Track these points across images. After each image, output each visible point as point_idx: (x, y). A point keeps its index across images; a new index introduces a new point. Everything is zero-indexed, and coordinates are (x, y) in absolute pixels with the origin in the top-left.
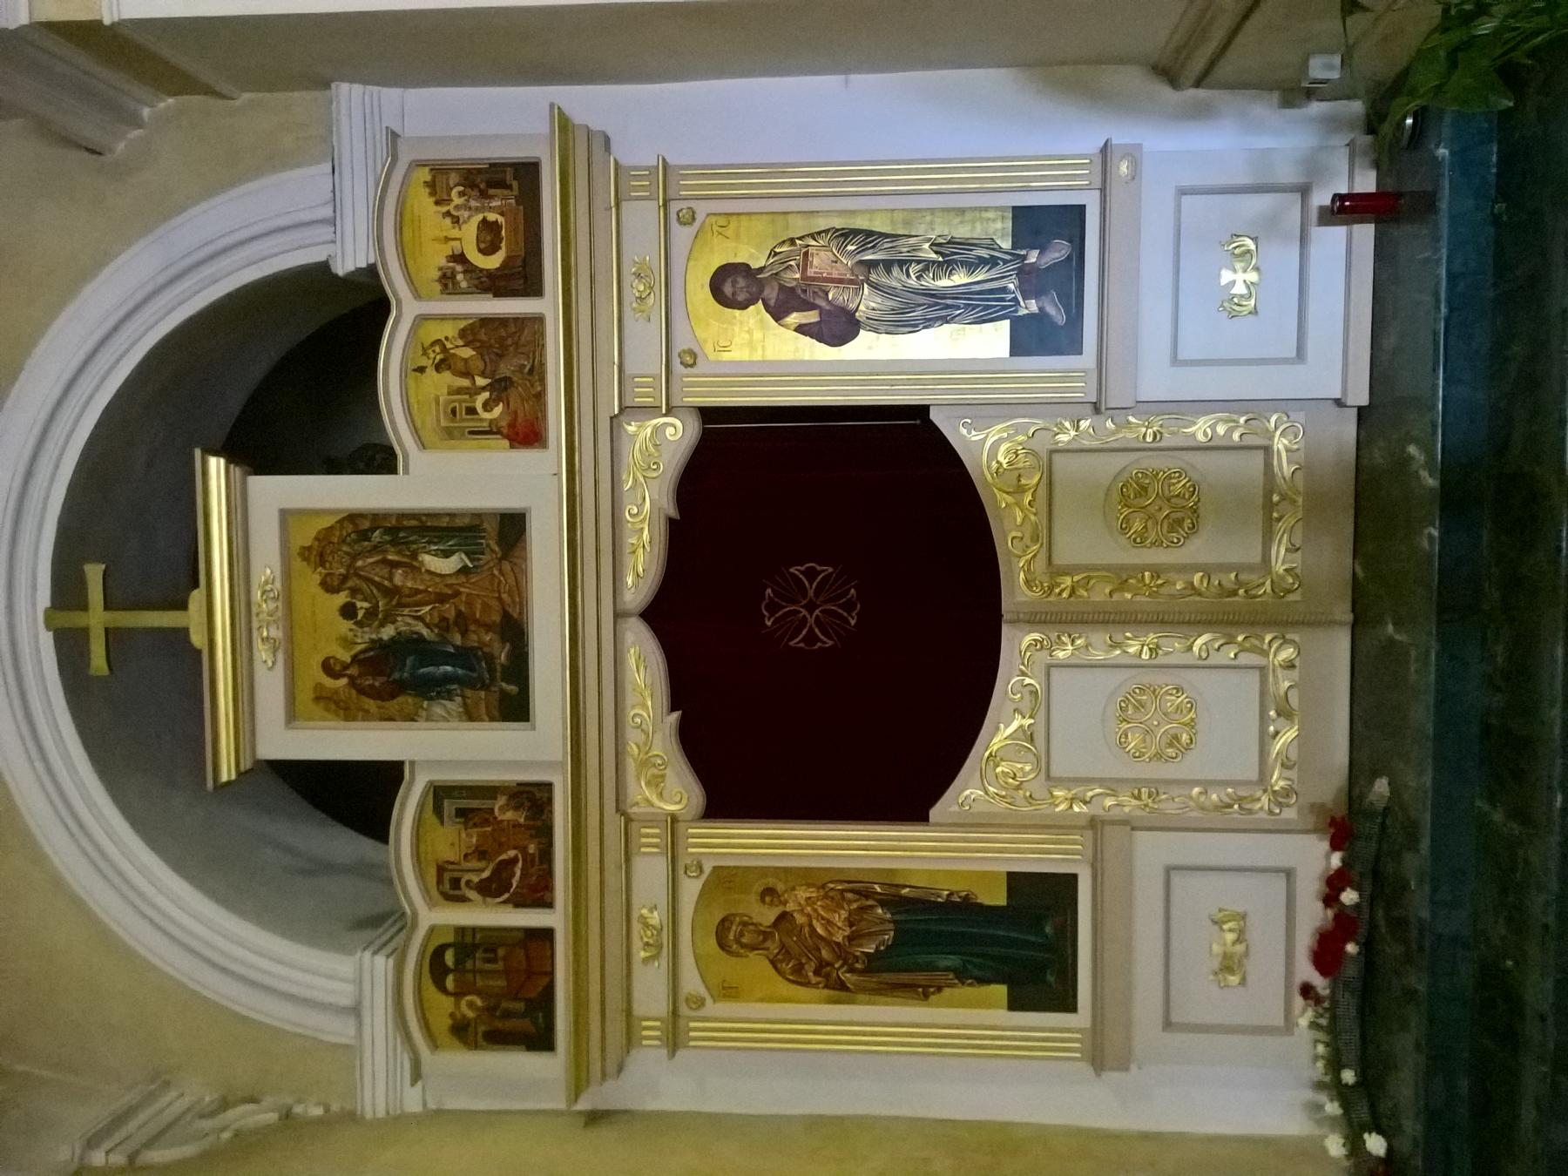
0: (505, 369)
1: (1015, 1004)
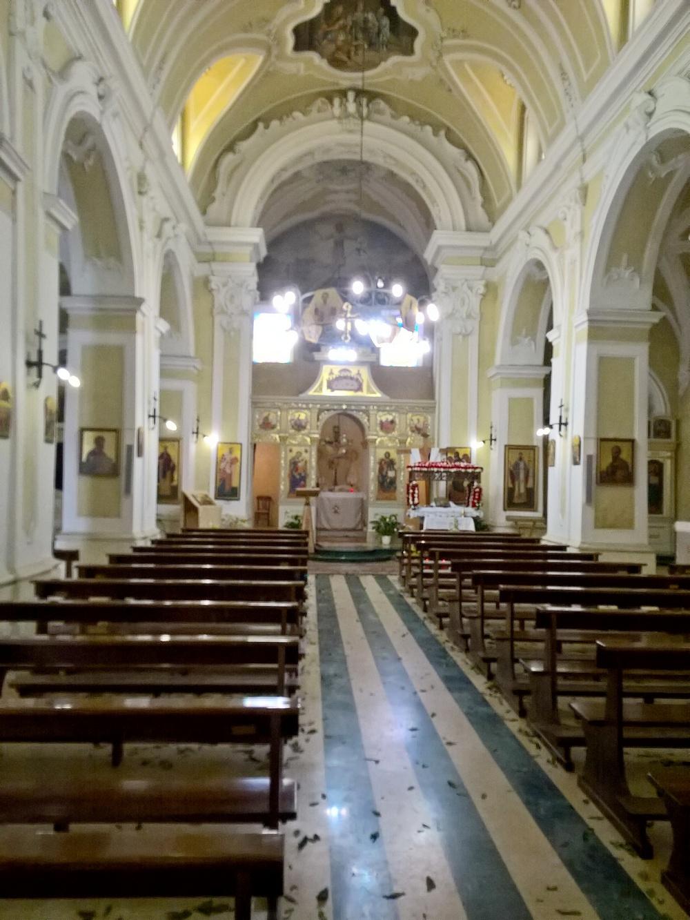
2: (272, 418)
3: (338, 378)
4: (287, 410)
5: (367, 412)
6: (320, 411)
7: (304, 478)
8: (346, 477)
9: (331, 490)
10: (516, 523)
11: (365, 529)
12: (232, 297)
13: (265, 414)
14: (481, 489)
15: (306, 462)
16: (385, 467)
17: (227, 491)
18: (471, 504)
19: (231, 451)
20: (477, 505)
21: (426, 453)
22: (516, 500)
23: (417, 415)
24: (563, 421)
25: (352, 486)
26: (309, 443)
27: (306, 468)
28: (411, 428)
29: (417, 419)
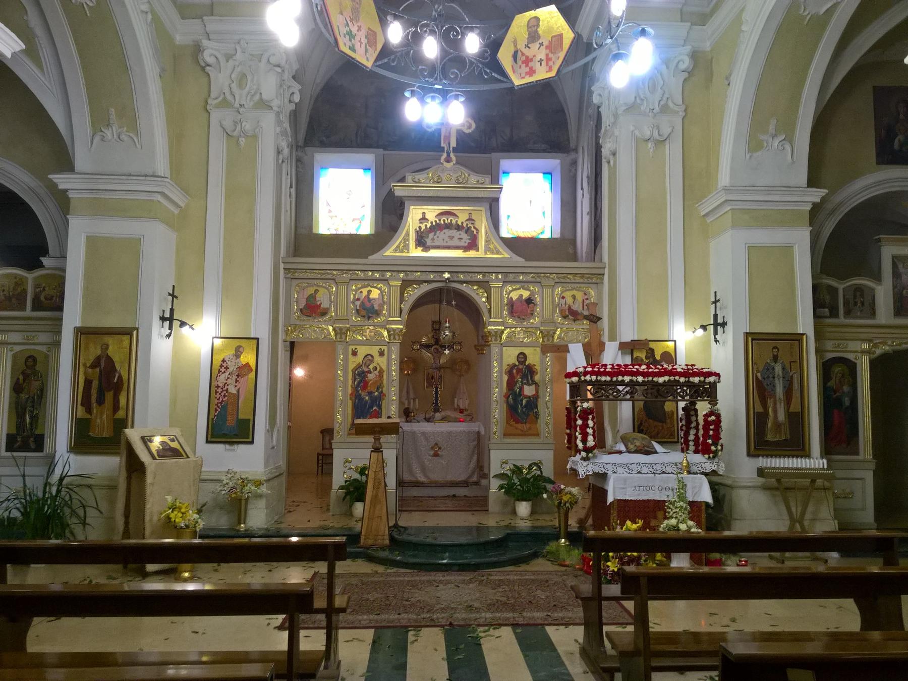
0: (14, 301)
1: (8, 435)
2: (323, 298)
3: (436, 228)
4: (347, 283)
5: (484, 285)
8: (454, 397)
9: (428, 420)
10: (779, 481)
11: (484, 482)
13: (311, 291)
14: (718, 416)
17: (228, 427)
18: (692, 448)
19: (238, 353)
20: (713, 448)
21: (592, 351)
22: (770, 437)
23: (573, 289)
24: (720, 320)
25: (461, 411)
27: (381, 383)
28: (561, 311)
29: (574, 297)
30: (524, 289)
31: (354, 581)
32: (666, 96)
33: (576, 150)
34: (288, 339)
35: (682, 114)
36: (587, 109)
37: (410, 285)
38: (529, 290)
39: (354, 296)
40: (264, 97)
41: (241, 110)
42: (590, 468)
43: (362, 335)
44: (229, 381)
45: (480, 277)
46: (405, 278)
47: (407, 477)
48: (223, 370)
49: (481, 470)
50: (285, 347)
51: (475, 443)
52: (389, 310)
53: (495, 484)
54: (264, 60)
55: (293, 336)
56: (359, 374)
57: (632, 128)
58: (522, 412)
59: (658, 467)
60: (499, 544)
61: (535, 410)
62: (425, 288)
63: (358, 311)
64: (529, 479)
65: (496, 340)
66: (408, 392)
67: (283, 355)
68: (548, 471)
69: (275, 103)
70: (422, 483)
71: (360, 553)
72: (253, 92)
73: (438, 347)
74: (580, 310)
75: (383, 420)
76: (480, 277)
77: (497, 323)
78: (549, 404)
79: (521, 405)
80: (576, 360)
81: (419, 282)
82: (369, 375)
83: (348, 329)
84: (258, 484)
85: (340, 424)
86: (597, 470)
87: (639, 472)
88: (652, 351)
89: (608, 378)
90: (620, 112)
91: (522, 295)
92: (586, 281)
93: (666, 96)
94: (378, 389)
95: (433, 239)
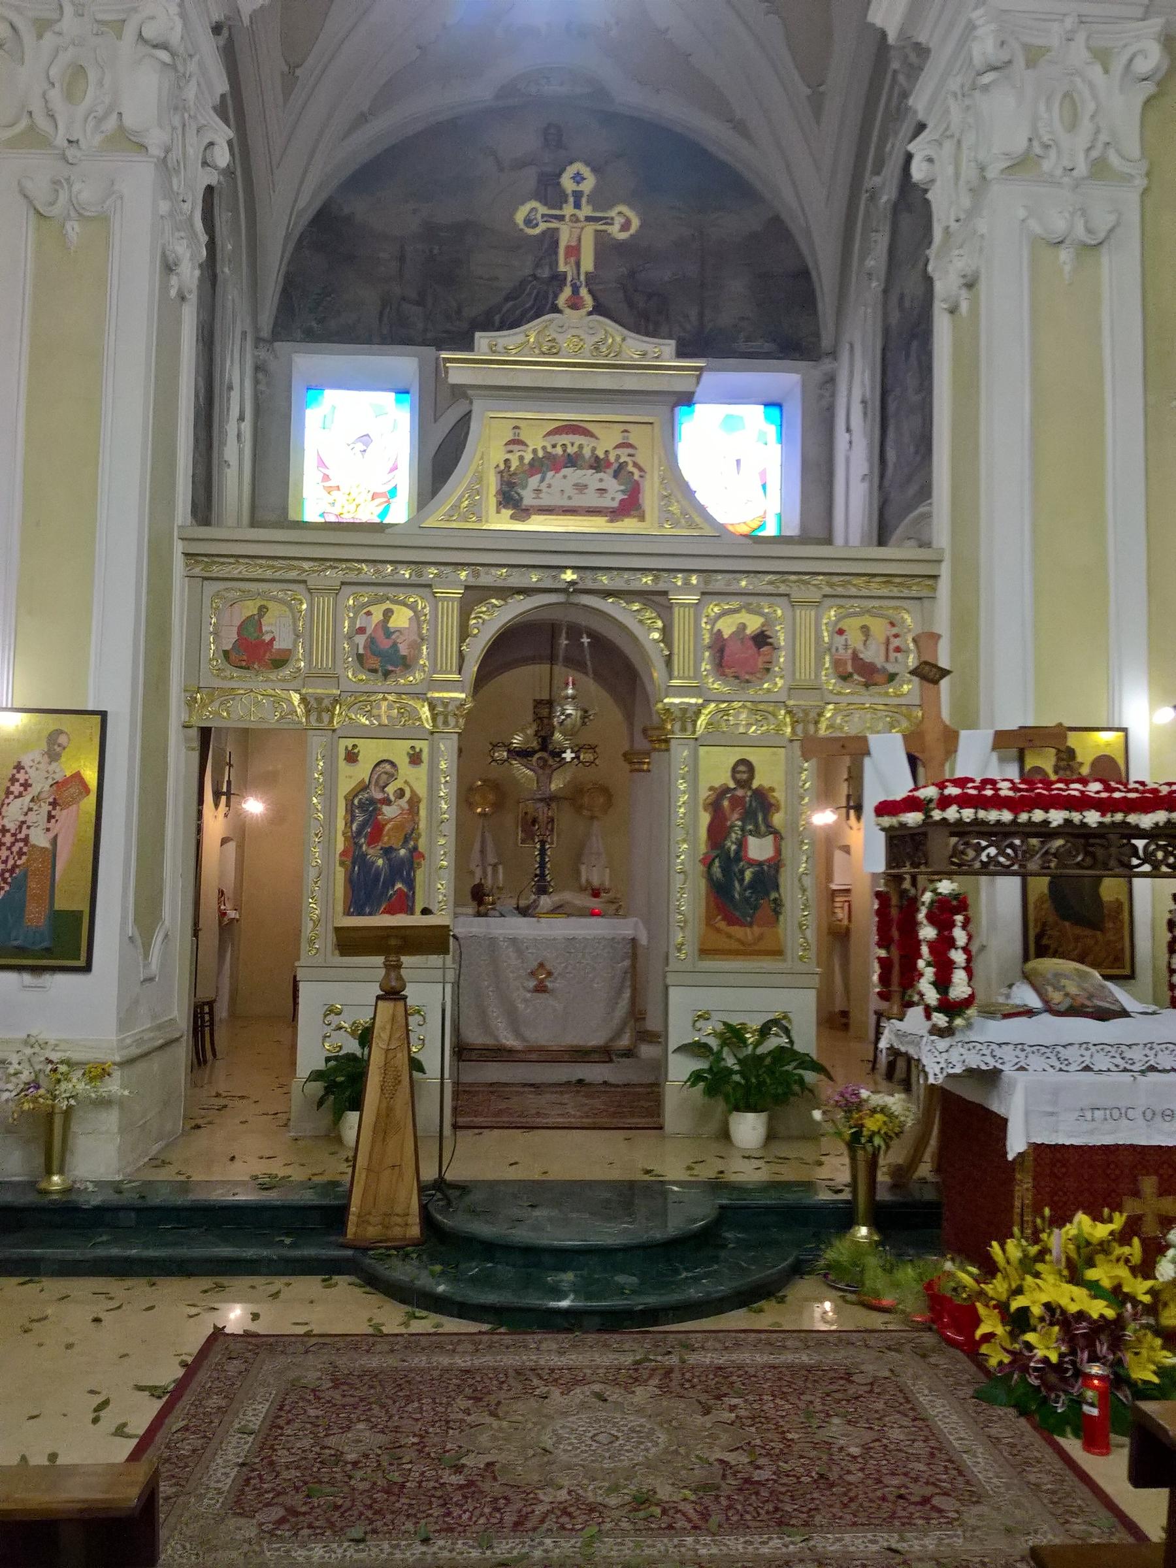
2: (278, 629)
3: (544, 464)
5: (657, 600)
6: (475, 595)
7: (404, 869)
9: (524, 912)
12: (78, 71)
15: (414, 802)
16: (735, 819)
25: (596, 894)
26: (428, 726)
28: (837, 663)
30: (750, 611)
31: (312, 1371)
32: (1103, 137)
33: (833, 354)
34: (197, 722)
35: (1140, 182)
36: (862, 259)
37: (480, 601)
38: (762, 614)
39: (352, 621)
40: (128, 122)
41: (71, 153)
42: (954, 1056)
43: (369, 714)
44: (31, 818)
45: (647, 580)
46: (472, 582)
47: (474, 1036)
48: (16, 788)
49: (641, 1026)
50: (187, 739)
51: (627, 963)
52: (433, 657)
53: (680, 1068)
54: (130, 32)
55: (213, 715)
56: (361, 805)
57: (1022, 213)
58: (742, 896)
59: (1136, 1054)
60: (699, 1244)
61: (773, 895)
62: (518, 607)
63: (360, 658)
64: (761, 1058)
65: (683, 729)
66: (483, 852)
67: (180, 757)
68: (806, 1039)
69: (156, 139)
70: (511, 1051)
71: (347, 1260)
72: (100, 110)
73: (545, 755)
74: (879, 661)
75: (416, 920)
76: (647, 580)
77: (684, 687)
78: (807, 881)
79: (742, 880)
80: (888, 774)
81: (506, 592)
82: (386, 809)
83: (336, 701)
84: (98, 1073)
85: (316, 923)
86: (974, 1061)
87: (1087, 1069)
88: (1071, 753)
89: (1007, 816)
90: (991, 174)
91: (743, 627)
92: (895, 592)
93: (1103, 137)
94: (406, 840)
95: (538, 491)
